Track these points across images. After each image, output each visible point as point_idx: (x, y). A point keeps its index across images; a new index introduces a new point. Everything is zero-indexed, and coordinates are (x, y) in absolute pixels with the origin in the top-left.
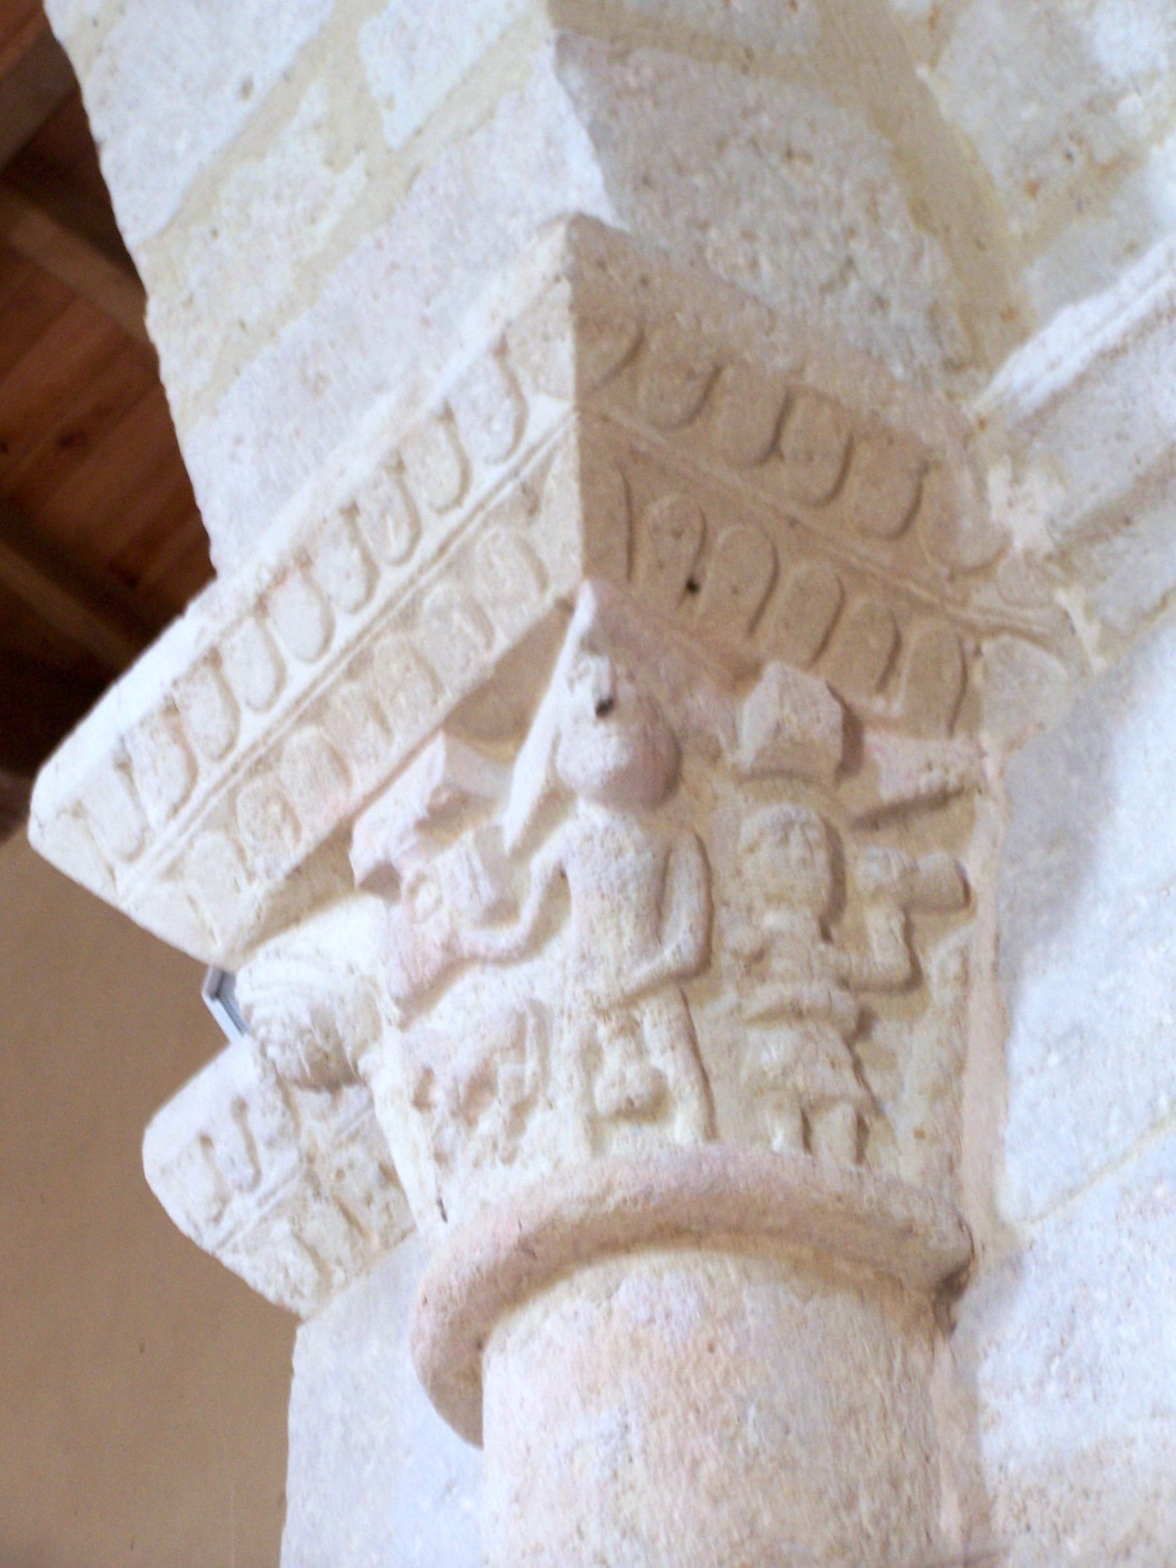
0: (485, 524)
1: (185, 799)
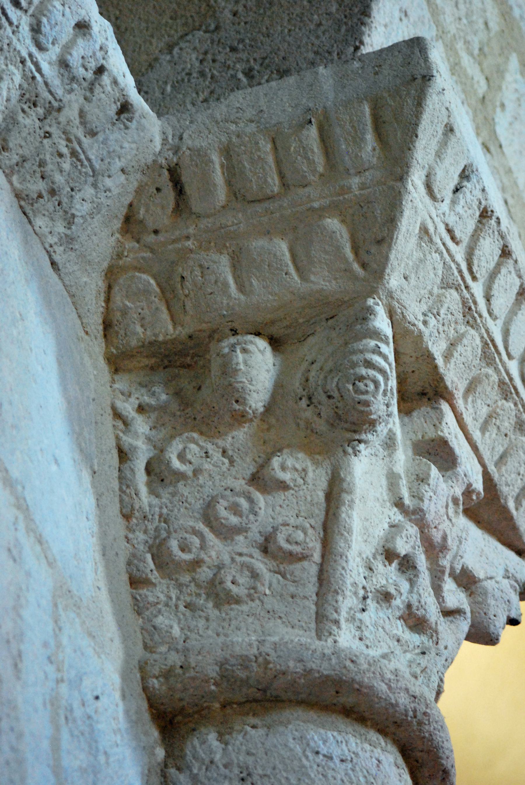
1: (453, 238)
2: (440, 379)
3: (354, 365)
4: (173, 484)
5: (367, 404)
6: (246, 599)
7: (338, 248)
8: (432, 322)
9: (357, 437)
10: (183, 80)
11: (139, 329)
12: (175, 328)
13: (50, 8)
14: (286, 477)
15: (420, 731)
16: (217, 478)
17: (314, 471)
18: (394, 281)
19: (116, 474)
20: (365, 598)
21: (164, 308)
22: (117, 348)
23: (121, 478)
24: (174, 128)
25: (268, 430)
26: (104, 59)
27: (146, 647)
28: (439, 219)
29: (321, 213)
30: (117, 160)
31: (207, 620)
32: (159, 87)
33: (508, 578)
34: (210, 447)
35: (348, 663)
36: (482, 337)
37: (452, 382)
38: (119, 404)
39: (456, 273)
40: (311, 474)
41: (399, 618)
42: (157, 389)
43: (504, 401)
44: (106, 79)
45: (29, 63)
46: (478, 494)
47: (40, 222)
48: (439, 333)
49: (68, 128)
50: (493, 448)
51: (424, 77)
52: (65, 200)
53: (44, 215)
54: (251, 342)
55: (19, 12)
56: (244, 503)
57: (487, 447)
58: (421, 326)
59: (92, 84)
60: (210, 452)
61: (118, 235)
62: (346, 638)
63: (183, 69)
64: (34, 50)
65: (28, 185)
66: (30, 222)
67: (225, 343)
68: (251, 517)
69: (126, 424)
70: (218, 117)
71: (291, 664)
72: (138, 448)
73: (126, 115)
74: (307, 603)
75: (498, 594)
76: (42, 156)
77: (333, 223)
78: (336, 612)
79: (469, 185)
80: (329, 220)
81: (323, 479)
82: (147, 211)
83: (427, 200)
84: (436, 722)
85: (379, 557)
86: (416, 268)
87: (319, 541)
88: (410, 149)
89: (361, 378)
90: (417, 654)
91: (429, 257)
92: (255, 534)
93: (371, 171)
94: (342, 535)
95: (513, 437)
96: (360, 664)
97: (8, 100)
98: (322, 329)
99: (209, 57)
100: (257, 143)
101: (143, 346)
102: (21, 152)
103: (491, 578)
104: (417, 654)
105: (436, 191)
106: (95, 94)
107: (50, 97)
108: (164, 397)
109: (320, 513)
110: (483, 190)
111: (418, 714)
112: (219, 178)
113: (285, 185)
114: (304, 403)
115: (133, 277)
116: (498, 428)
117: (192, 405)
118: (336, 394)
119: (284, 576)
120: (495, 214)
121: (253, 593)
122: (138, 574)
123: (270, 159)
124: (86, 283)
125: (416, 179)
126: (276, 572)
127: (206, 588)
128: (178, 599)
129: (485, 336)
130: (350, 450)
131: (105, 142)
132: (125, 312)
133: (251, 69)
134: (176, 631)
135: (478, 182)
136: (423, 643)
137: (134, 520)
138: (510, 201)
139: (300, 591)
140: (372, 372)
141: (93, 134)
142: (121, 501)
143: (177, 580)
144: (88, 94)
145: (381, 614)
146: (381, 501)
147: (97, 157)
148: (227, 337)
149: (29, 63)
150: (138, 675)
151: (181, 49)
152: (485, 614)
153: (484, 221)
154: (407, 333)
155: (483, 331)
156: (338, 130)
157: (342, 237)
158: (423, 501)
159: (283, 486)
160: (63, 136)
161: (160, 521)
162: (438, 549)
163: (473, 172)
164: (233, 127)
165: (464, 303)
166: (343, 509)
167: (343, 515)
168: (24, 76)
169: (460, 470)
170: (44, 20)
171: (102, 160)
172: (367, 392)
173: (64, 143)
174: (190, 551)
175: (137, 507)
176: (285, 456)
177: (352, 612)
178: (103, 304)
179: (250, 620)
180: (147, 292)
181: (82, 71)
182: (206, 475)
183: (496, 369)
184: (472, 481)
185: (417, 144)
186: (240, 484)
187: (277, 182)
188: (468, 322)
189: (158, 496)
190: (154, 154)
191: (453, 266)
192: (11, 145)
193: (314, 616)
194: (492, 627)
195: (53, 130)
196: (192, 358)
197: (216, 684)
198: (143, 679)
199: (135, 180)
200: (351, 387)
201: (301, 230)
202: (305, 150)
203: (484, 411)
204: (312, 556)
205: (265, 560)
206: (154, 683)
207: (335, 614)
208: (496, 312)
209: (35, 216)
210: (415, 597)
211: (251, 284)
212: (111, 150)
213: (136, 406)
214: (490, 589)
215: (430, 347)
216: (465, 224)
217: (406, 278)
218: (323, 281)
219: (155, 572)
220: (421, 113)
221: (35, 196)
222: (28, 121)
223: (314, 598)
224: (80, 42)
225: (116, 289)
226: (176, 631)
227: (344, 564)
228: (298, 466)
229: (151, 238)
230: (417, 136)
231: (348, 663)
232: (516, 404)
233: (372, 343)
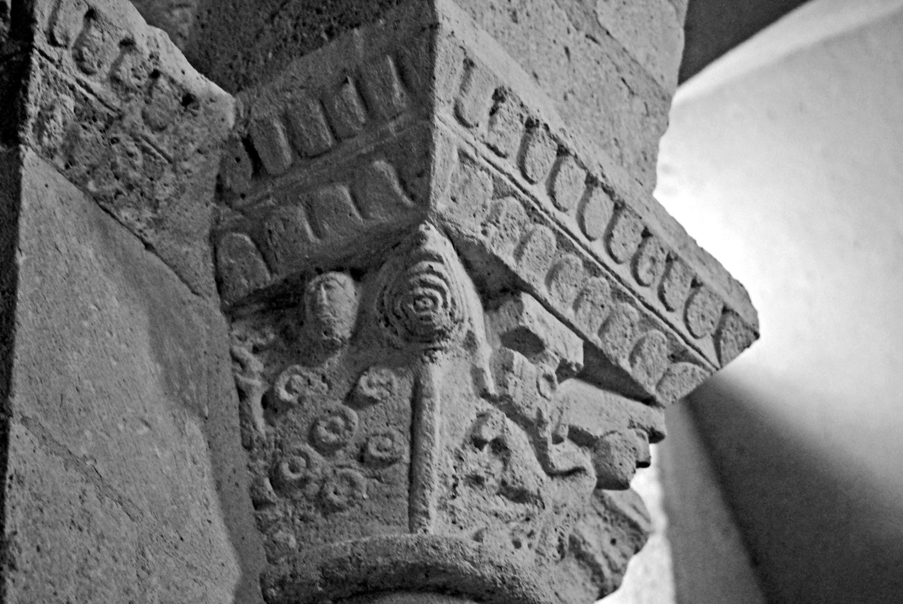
0: (666, 333)
1: (498, 154)
2: (515, 276)
3: (412, 287)
4: (284, 412)
5: (429, 318)
6: (346, 505)
7: (388, 186)
8: (492, 230)
9: (432, 346)
10: (281, 46)
11: (244, 281)
12: (271, 276)
13: (88, 37)
14: (373, 392)
15: (513, 594)
16: (319, 401)
17: (399, 382)
18: (441, 205)
19: (236, 412)
20: (455, 486)
21: (261, 262)
22: (229, 301)
23: (242, 415)
24: (245, 104)
25: (357, 352)
26: (156, 64)
27: (269, 560)
28: (478, 141)
29: (368, 158)
30: (190, 145)
31: (317, 528)
32: (263, 55)
33: (634, 427)
34: (311, 375)
35: (431, 551)
36: (554, 230)
37: (528, 276)
38: (236, 349)
39: (509, 182)
40: (396, 385)
41: (498, 494)
42: (267, 330)
43: (594, 278)
44: (162, 81)
45: (78, 88)
46: (577, 365)
47: (125, 214)
48: (502, 237)
49: (133, 130)
50: (590, 321)
51: (431, 26)
52: (146, 190)
53: (129, 207)
54: (332, 278)
55: (58, 49)
56: (339, 421)
57: (582, 322)
58: (481, 237)
59: (150, 88)
60: (312, 379)
61: (213, 204)
62: (436, 525)
63: (280, 36)
64: (82, 76)
65: (104, 187)
66: (113, 216)
67: (312, 283)
68: (347, 432)
69: (243, 366)
70: (278, 87)
71: (380, 560)
72: (253, 386)
73: (192, 105)
74: (400, 500)
75: (621, 445)
76: (112, 160)
77: (380, 165)
78: (424, 504)
79: (504, 105)
80: (377, 163)
81: (408, 388)
82: (232, 179)
83: (461, 128)
84: (528, 583)
85: (467, 447)
86: (463, 189)
87: (408, 442)
88: (430, 90)
89: (420, 298)
90: (522, 522)
91: (474, 176)
92: (352, 448)
93: (404, 115)
94: (425, 435)
95: (613, 305)
96: (442, 549)
97: (65, 123)
98: (387, 258)
99: (301, 21)
100: (308, 107)
101: (250, 295)
102: (88, 162)
103: (612, 432)
104: (522, 522)
105: (467, 119)
106: (154, 96)
107: (108, 110)
108: (272, 336)
109: (407, 418)
110: (522, 105)
111: (507, 580)
112: (283, 141)
113: (337, 138)
114: (382, 324)
115: (232, 237)
116: (592, 302)
117: (296, 339)
118: (401, 314)
119: (379, 479)
120: (541, 122)
121: (352, 500)
122: (259, 498)
123: (321, 118)
124: (187, 253)
125: (443, 114)
126: (372, 478)
127: (315, 500)
128: (294, 513)
129: (557, 227)
130: (427, 359)
131: (175, 132)
132: (230, 268)
133: (331, 28)
134: (293, 542)
135: (514, 100)
136: (527, 510)
137: (255, 449)
138: (628, 78)
139: (394, 491)
140: (428, 291)
141: (161, 129)
142: (242, 435)
143: (291, 497)
144: (148, 97)
145: (475, 496)
146: (467, 395)
147: (169, 148)
148: (315, 276)
149: (78, 88)
150: (259, 588)
151: (280, 17)
152: (611, 465)
153: (532, 130)
154: (469, 245)
155: (553, 224)
156: (370, 84)
157: (389, 175)
158: (507, 387)
159: (372, 401)
160: (131, 138)
161: (276, 447)
162: (535, 425)
163: (506, 93)
164: (288, 95)
165: (525, 205)
166: (425, 412)
167: (425, 418)
168: (77, 99)
169: (549, 351)
170: (85, 49)
171: (175, 148)
172: (426, 309)
173: (133, 143)
174: (298, 471)
175: (255, 438)
176: (371, 374)
177: (443, 500)
178: (212, 265)
179: (351, 523)
180: (244, 248)
181: (134, 81)
182: (310, 402)
183: (578, 254)
184: (565, 357)
185: (436, 85)
186: (337, 404)
187: (329, 137)
188: (535, 220)
189: (273, 425)
190: (229, 130)
191: (504, 177)
192: (76, 159)
193: (407, 511)
194: (619, 475)
195: (121, 135)
196: (295, 298)
197: (321, 585)
198: (263, 590)
199: (215, 157)
200: (412, 307)
201: (356, 173)
202: (347, 105)
203: (572, 293)
204: (401, 457)
205: (362, 469)
206: (272, 593)
207: (424, 507)
208: (563, 204)
209: (117, 210)
210: (508, 474)
211: (323, 227)
212: (182, 137)
213: (251, 348)
214: (612, 443)
215: (495, 253)
216: (509, 140)
217: (454, 200)
218: (381, 217)
219: (273, 493)
220: (434, 58)
221: (113, 194)
222: (89, 136)
223: (407, 493)
224: (127, 57)
225: (220, 250)
226: (293, 542)
227: (429, 461)
228: (383, 381)
229: (240, 202)
230: (434, 78)
231: (431, 551)
232: (607, 277)
233: (426, 264)
